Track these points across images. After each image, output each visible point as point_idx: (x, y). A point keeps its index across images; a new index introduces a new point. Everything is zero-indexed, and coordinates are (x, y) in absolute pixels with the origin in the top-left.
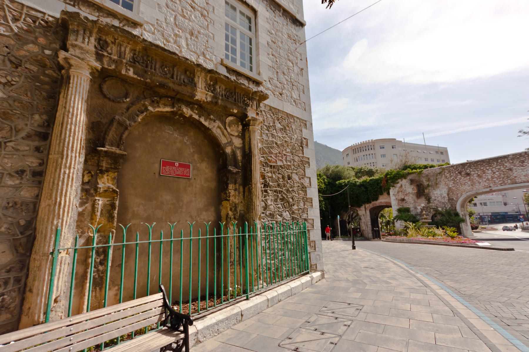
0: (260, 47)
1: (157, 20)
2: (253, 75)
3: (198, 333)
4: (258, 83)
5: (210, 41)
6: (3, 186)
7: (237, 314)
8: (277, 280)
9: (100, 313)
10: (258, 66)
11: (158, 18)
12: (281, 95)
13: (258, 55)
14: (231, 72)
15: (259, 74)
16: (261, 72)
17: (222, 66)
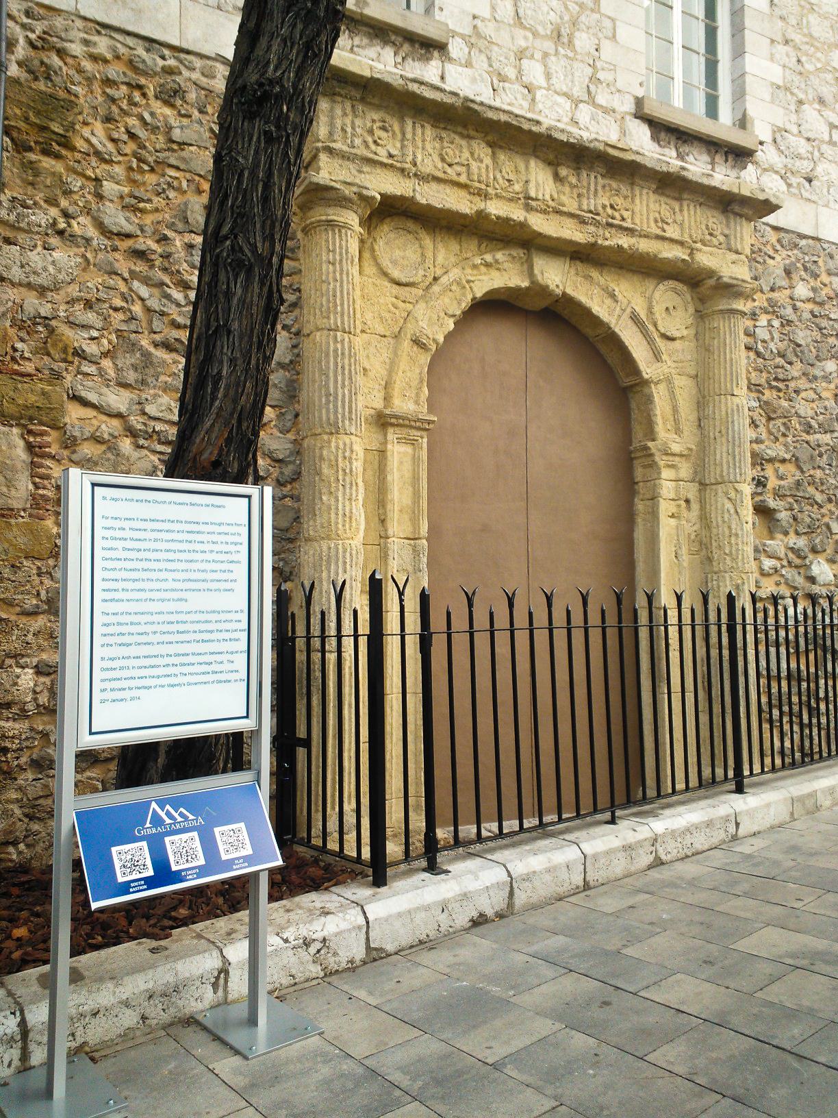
0: (748, 23)
1: (474, 17)
2: (723, 127)
3: (656, 840)
4: (739, 155)
5: (607, 46)
6: (203, 89)
7: (726, 819)
8: (511, 825)
9: (416, 762)
10: (739, 94)
11: (477, 13)
12: (810, 181)
13: (739, 52)
14: (663, 135)
15: (743, 123)
16: (751, 112)
17: (638, 121)
